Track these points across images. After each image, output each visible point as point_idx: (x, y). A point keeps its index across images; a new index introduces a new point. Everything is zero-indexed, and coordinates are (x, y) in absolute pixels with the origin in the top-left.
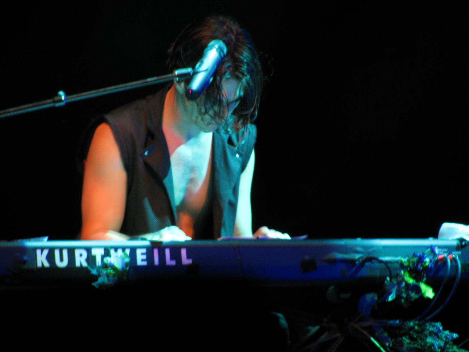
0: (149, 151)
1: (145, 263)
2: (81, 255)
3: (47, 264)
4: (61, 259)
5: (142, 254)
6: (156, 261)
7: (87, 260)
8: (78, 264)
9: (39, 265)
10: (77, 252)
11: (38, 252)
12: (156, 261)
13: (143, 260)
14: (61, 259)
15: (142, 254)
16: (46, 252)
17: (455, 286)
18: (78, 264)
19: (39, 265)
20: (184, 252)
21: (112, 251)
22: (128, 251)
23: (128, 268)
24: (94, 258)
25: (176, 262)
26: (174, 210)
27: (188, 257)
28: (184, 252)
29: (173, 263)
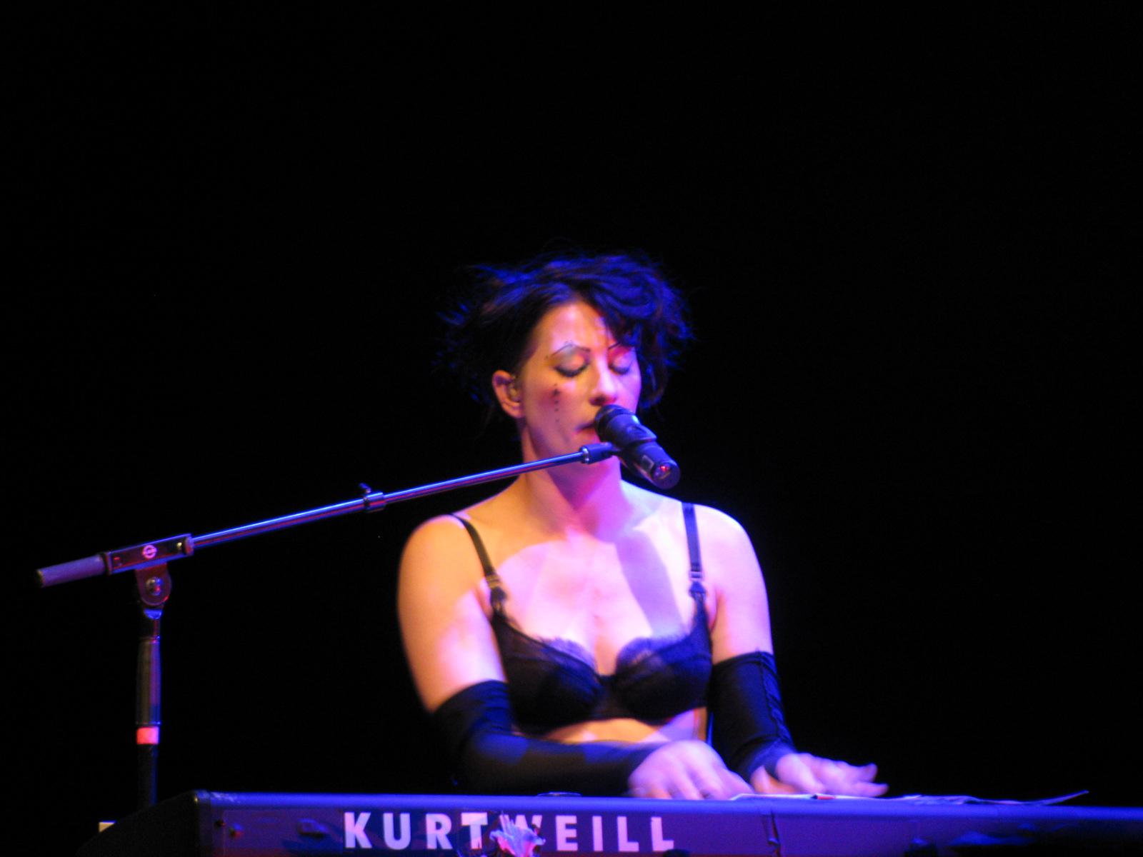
0: (879, 767)
1: (573, 847)
2: (438, 826)
3: (365, 844)
4: (397, 835)
5: (568, 826)
6: (598, 845)
7: (450, 837)
8: (431, 845)
9: (350, 844)
10: (431, 820)
11: (349, 817)
12: (598, 845)
13: (569, 840)
14: (397, 835)
15: (568, 826)
16: (364, 817)
17: (1080, 794)
18: (431, 845)
19: (350, 844)
20: (656, 823)
21: (504, 819)
22: (537, 820)
23: (139, 601)
24: (466, 830)
25: (640, 846)
26: (752, 795)
27: (666, 836)
28: (656, 823)
29: (634, 847)
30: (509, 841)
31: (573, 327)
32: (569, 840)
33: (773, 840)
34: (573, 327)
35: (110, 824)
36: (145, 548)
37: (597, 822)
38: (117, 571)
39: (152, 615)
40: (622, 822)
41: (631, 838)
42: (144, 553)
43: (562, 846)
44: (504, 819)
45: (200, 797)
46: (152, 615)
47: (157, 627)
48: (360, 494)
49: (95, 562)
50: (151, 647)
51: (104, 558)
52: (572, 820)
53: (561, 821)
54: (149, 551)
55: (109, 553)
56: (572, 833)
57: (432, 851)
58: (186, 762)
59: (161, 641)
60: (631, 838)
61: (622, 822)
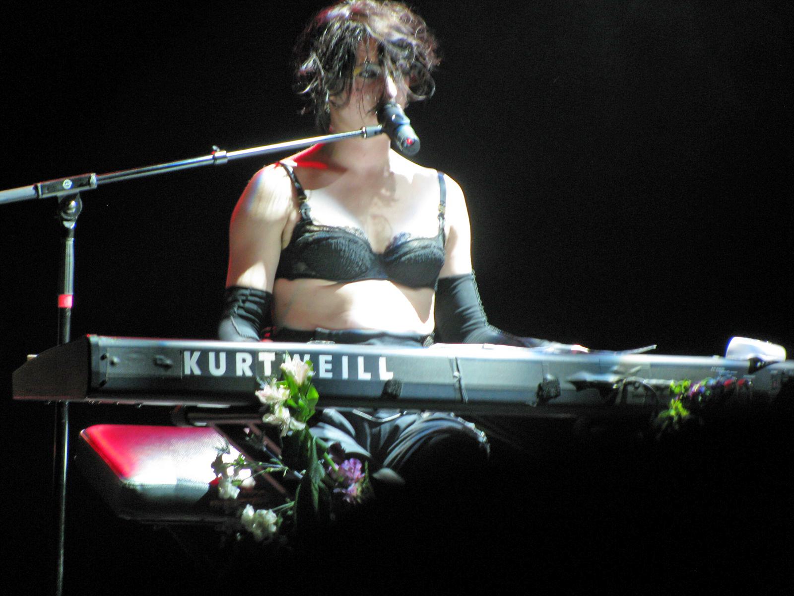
1: (330, 375)
2: (244, 361)
3: (197, 372)
4: (217, 366)
5: (327, 362)
6: (345, 375)
8: (239, 373)
11: (187, 354)
13: (327, 371)
14: (217, 366)
15: (327, 362)
16: (197, 355)
18: (239, 373)
19: (187, 372)
27: (388, 370)
30: (219, 441)
31: (656, 345)
32: (327, 371)
33: (456, 374)
34: (656, 345)
35: (35, 356)
36: (65, 182)
37: (345, 360)
38: (45, 196)
39: (70, 225)
40: (361, 361)
41: (366, 370)
42: (64, 185)
43: (323, 374)
44: (287, 357)
45: (94, 339)
46: (70, 225)
47: (72, 233)
48: (210, 151)
49: (27, 191)
50: (70, 242)
51: (36, 188)
52: (330, 358)
53: (322, 359)
54: (67, 183)
55: (39, 185)
56: (329, 366)
57: (239, 378)
58: (90, 318)
59: (74, 242)
60: (366, 370)
61: (361, 361)
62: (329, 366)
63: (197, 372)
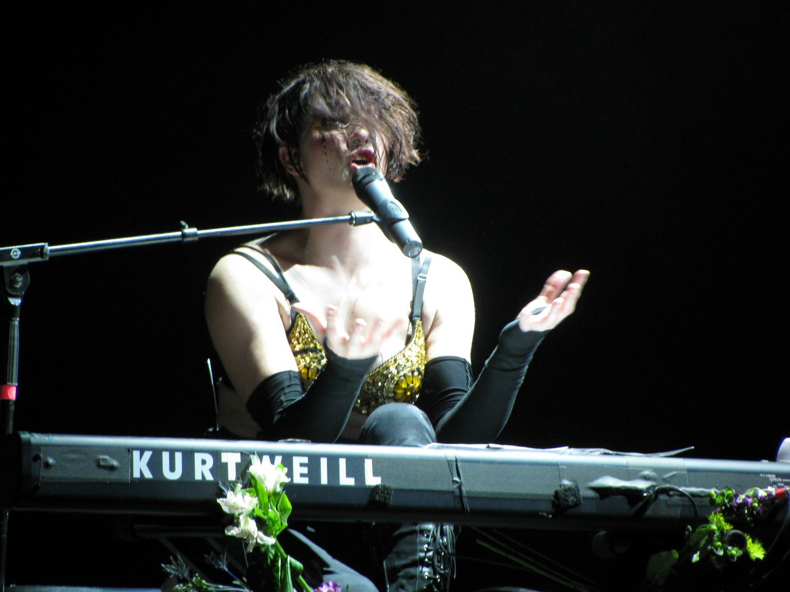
2: (204, 462)
4: (172, 469)
5: (302, 465)
8: (198, 477)
9: (136, 475)
13: (302, 475)
14: (172, 469)
15: (302, 465)
18: (198, 477)
24: (225, 465)
32: (302, 475)
57: (198, 482)
62: (305, 470)
63: (148, 475)
